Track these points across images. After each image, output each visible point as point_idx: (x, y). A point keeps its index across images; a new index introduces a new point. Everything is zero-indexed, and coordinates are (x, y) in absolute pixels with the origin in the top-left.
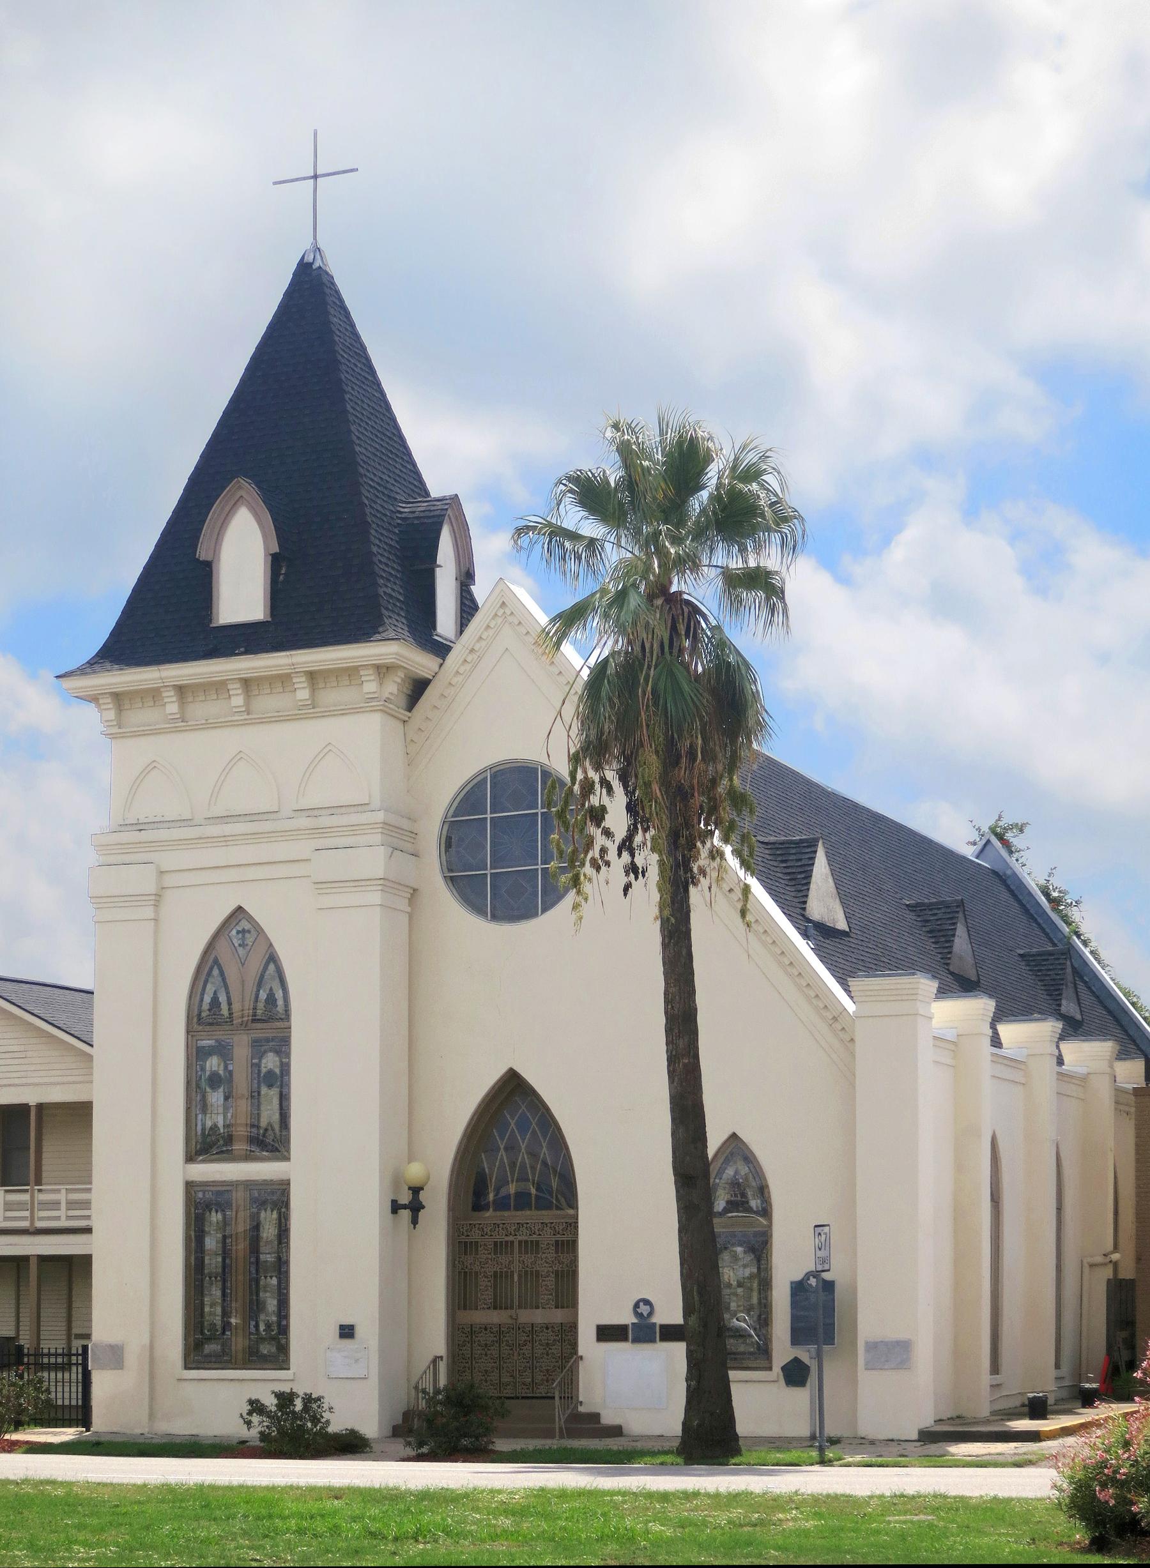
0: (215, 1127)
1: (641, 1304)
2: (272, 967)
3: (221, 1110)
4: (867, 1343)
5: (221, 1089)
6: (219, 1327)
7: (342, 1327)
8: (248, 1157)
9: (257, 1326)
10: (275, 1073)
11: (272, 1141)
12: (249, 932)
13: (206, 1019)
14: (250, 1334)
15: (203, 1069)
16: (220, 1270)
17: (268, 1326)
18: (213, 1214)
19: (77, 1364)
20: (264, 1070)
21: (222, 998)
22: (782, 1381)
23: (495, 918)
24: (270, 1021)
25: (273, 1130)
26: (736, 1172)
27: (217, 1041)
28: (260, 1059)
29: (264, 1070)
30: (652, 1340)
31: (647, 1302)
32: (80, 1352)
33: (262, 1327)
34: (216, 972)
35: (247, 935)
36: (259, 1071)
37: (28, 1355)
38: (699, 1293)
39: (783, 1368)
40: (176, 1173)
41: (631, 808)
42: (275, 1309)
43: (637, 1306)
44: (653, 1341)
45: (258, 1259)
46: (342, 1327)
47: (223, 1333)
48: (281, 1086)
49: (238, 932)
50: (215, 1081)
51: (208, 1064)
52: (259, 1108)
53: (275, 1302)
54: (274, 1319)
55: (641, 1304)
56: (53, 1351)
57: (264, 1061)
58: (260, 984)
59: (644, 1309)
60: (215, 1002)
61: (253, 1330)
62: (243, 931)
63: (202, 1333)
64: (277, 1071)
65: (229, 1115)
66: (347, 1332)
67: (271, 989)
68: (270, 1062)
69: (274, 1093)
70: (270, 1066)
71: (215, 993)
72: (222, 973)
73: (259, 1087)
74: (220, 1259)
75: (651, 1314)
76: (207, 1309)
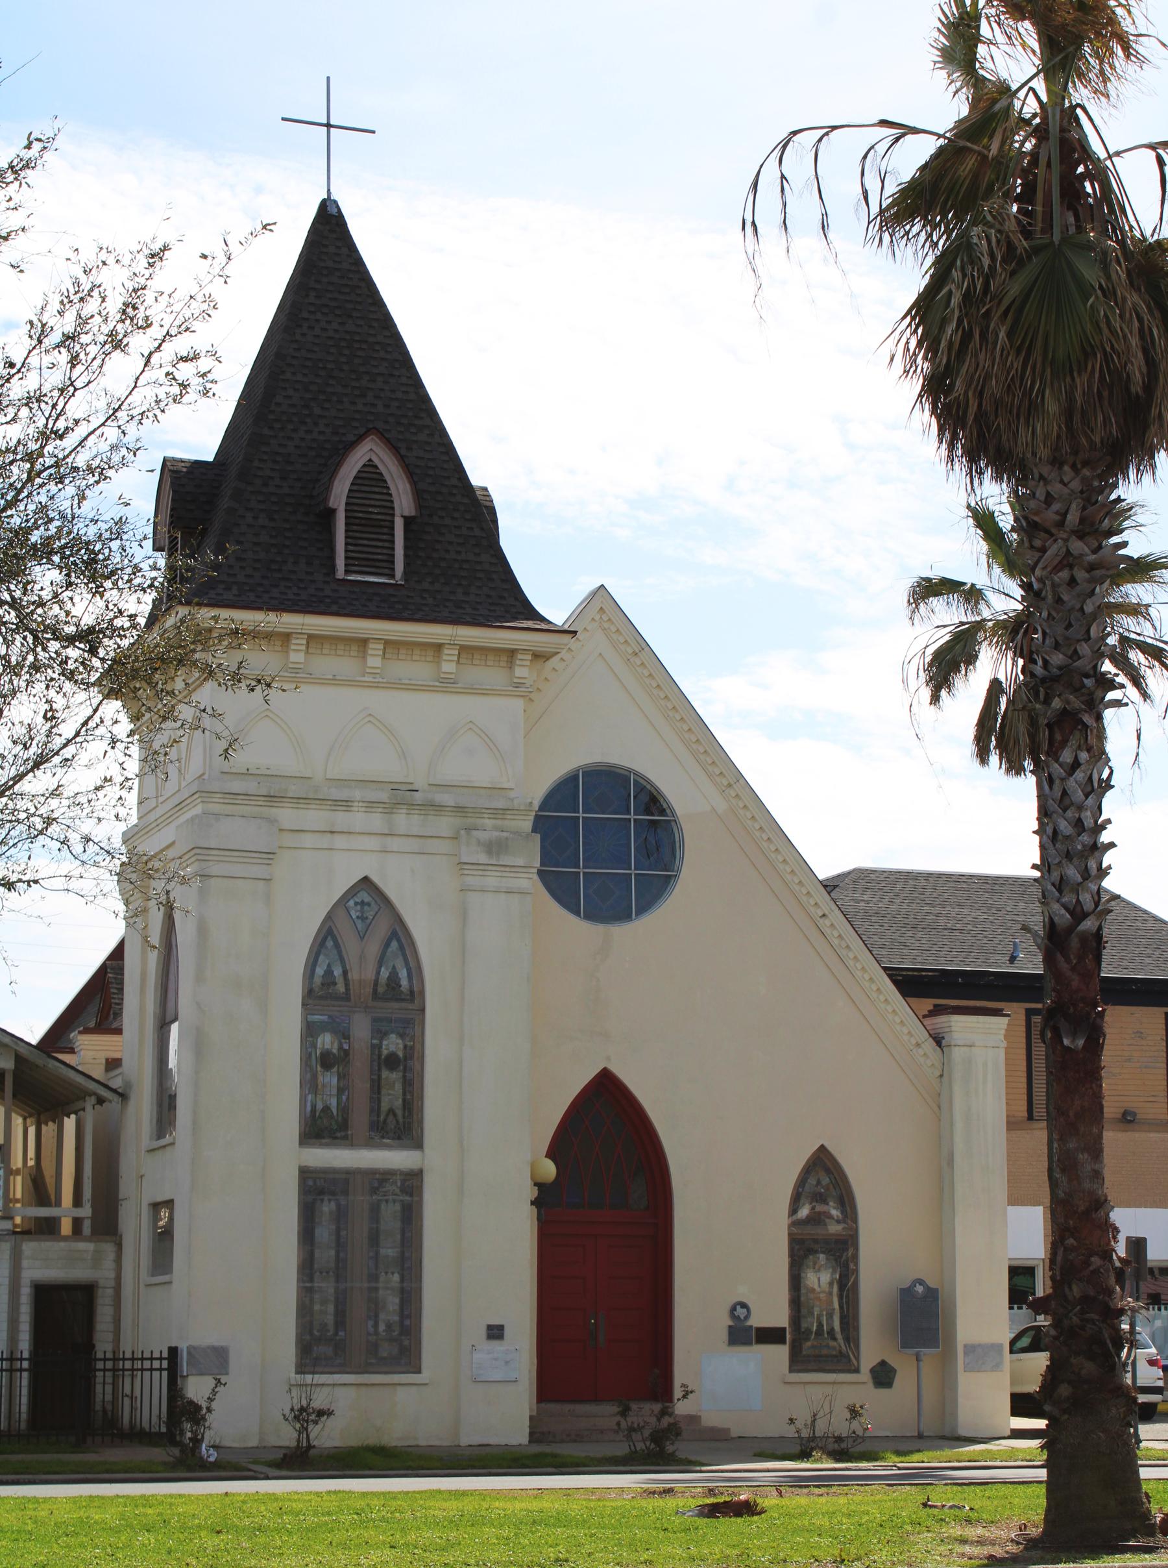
0: (326, 1109)
1: (738, 1307)
2: (394, 944)
3: (334, 1092)
4: (965, 1346)
5: (335, 1069)
6: (331, 1327)
7: (490, 1328)
8: (369, 1144)
9: (376, 1325)
10: (397, 1056)
11: (404, 1126)
12: (369, 904)
13: (323, 994)
14: (369, 1334)
15: (314, 1046)
16: (333, 1265)
17: (389, 1326)
18: (326, 1202)
19: (161, 1369)
20: (385, 1052)
21: (337, 972)
22: (871, 1385)
23: (589, 917)
24: (398, 999)
25: (395, 1115)
26: (819, 1183)
27: (330, 1017)
28: (381, 1040)
29: (385, 1052)
30: (747, 1343)
31: (744, 1305)
32: (165, 1355)
33: (382, 1327)
34: (330, 943)
35: (366, 908)
36: (380, 1056)
37: (105, 1360)
38: (840, 1297)
39: (872, 1371)
40: (288, 1156)
41: (144, 760)
42: (397, 1307)
43: (734, 1309)
44: (750, 1344)
45: (377, 1253)
46: (490, 1328)
47: (336, 1334)
48: (405, 1071)
49: (356, 904)
50: (392, 1062)
51: (320, 1040)
52: (379, 1092)
53: (397, 1301)
54: (397, 1318)
55: (738, 1307)
56: (147, 1355)
57: (385, 1043)
58: (381, 962)
59: (741, 1312)
60: (329, 972)
61: (371, 1330)
62: (363, 903)
63: (311, 1334)
64: (401, 1054)
65: (344, 1098)
66: (495, 1332)
67: (394, 967)
68: (393, 1044)
69: (395, 1076)
70: (392, 1048)
71: (329, 966)
72: (337, 945)
73: (380, 1070)
74: (333, 1253)
75: (747, 1317)
76: (317, 1307)
